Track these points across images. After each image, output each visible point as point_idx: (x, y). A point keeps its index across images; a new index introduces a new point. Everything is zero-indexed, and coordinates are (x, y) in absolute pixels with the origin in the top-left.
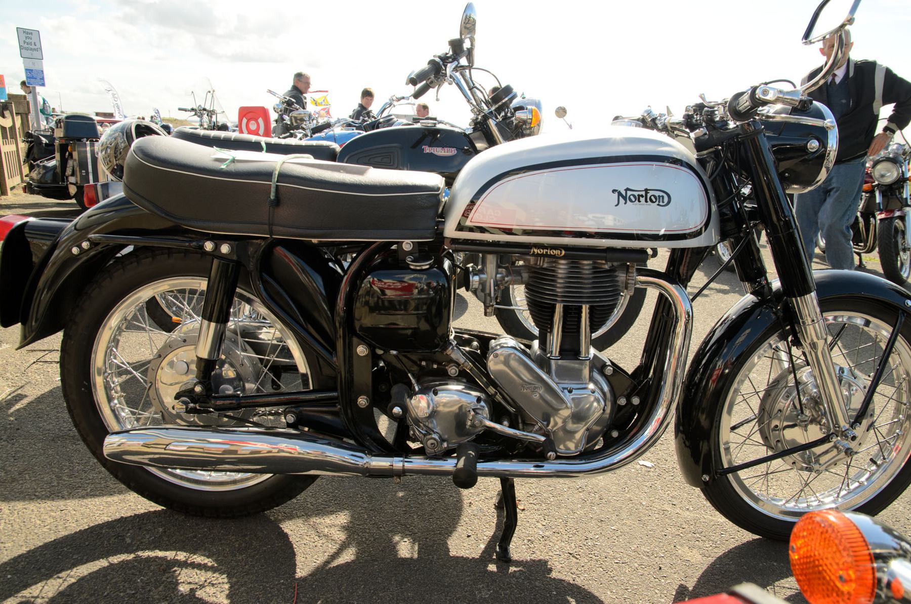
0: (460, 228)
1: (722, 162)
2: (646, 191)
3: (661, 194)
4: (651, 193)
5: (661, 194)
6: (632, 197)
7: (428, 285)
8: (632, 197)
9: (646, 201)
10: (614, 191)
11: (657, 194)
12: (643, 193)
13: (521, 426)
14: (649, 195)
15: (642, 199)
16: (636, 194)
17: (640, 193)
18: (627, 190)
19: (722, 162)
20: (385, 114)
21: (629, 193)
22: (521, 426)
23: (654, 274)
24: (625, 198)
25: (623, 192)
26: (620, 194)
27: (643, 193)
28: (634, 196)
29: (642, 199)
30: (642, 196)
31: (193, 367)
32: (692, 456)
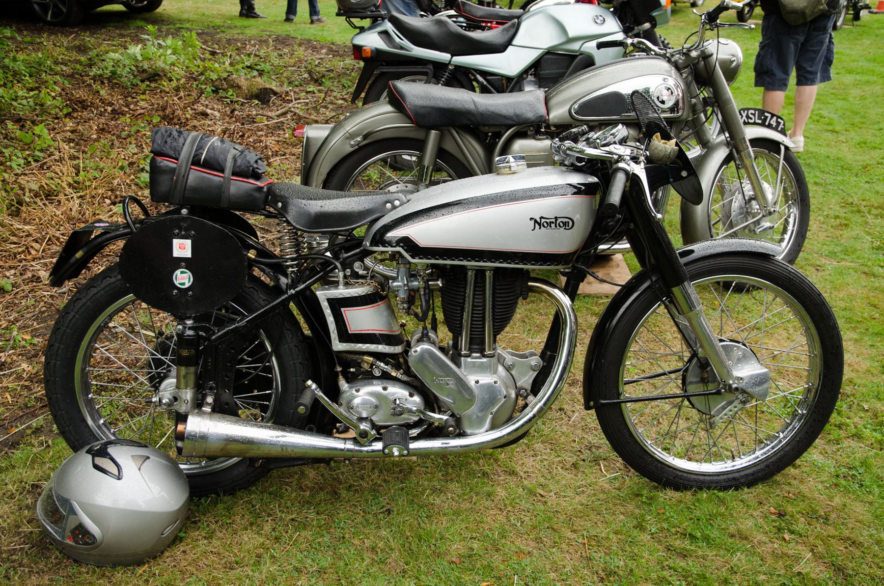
0: (337, 304)
1: (219, 334)
2: (556, 218)
3: (567, 220)
4: (560, 220)
5: (567, 220)
6: (545, 224)
7: (100, 221)
8: (545, 224)
9: (556, 226)
10: (531, 219)
11: (564, 220)
12: (554, 220)
13: (437, 411)
14: (558, 222)
15: (553, 225)
16: (548, 221)
17: (551, 220)
18: (541, 218)
19: (219, 334)
20: (269, 482)
21: (543, 220)
22: (437, 411)
23: (479, 281)
24: (539, 224)
25: (539, 220)
26: (536, 221)
27: (554, 220)
28: (546, 222)
29: (553, 225)
30: (553, 222)
31: (494, 170)
32: (408, 237)
